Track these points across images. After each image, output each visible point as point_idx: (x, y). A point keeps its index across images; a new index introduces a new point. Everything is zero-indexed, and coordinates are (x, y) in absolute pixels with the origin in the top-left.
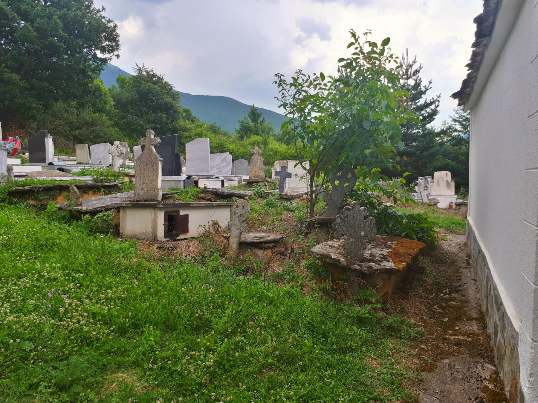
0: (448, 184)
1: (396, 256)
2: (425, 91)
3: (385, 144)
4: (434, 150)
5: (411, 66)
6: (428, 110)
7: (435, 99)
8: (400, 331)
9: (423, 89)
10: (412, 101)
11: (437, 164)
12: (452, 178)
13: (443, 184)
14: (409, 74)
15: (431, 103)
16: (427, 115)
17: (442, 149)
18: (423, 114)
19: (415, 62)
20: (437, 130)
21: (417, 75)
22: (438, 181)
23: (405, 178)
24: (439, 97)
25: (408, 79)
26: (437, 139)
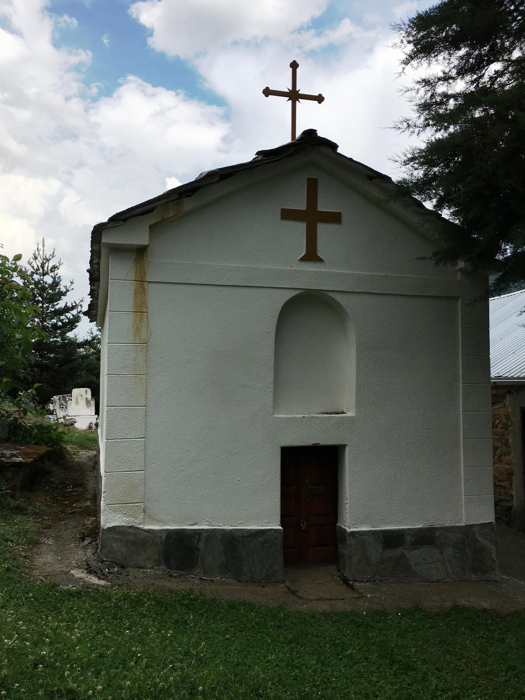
0: (88, 402)
1: (25, 454)
2: (66, 293)
3: (16, 356)
4: (75, 363)
5: (48, 260)
6: (69, 315)
7: (77, 304)
8: (27, 510)
9: (63, 290)
10: (49, 303)
11: (79, 381)
12: (92, 396)
13: (83, 402)
14: (46, 269)
15: (73, 308)
16: (67, 321)
17: (85, 364)
18: (63, 320)
19: (53, 256)
20: (80, 340)
21: (56, 272)
22: (77, 398)
23: (35, 389)
24: (82, 301)
25: (44, 274)
26: (81, 350)
